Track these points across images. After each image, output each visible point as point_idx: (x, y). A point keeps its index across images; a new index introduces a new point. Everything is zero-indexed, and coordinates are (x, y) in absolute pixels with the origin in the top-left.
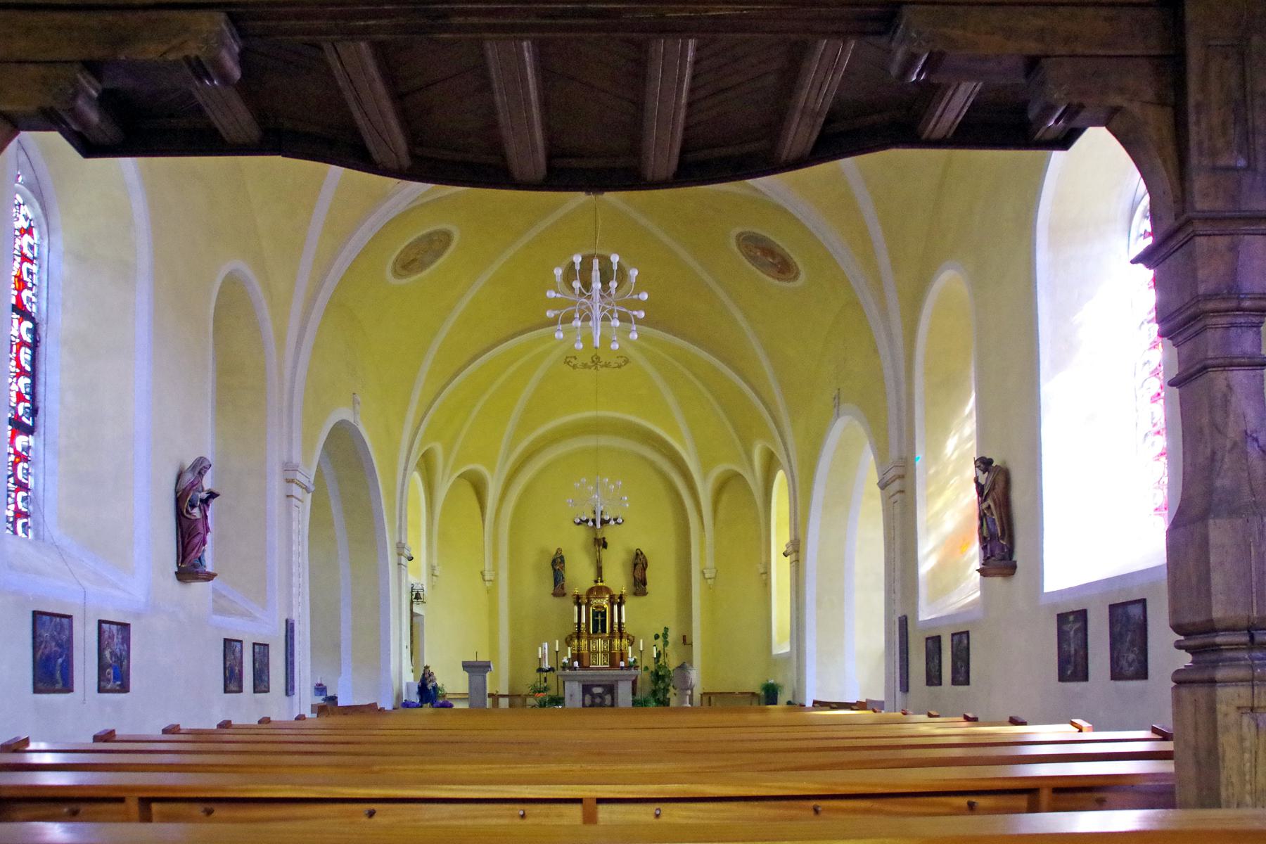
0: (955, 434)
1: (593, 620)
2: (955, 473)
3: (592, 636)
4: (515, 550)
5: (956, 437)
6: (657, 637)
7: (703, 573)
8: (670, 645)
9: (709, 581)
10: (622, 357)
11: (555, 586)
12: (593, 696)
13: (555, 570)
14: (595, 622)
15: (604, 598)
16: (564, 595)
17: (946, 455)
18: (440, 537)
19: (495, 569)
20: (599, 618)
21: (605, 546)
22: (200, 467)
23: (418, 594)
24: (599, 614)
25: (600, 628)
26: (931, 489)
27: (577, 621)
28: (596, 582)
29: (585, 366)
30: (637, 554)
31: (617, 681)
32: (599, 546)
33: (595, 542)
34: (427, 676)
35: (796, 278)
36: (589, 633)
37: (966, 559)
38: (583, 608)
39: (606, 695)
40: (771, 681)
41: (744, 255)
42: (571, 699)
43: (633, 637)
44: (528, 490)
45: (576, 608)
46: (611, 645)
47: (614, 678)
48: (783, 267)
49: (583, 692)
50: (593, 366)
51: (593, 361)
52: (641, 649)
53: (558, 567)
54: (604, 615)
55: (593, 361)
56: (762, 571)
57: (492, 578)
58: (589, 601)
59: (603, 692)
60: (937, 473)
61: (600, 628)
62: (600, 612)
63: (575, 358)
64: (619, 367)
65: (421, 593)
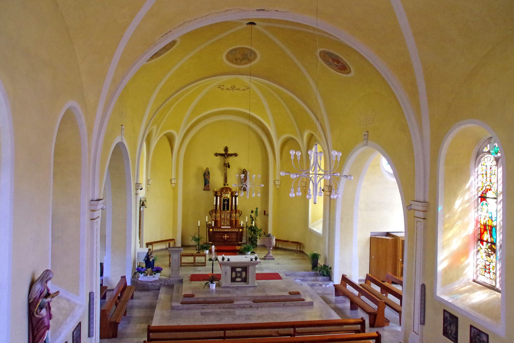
0: (460, 198)
1: (223, 203)
2: (459, 218)
4: (186, 167)
5: (461, 199)
6: (252, 212)
7: (274, 181)
9: (277, 186)
10: (246, 87)
11: (205, 185)
13: (205, 178)
14: (224, 205)
15: (228, 194)
16: (209, 190)
17: (455, 208)
18: (152, 167)
19: (177, 179)
21: (229, 167)
22: (46, 276)
23: (143, 203)
24: (226, 201)
25: (226, 208)
26: (446, 226)
28: (225, 185)
29: (228, 89)
30: (244, 171)
31: (249, 266)
32: (226, 167)
33: (224, 165)
34: (149, 254)
35: (350, 72)
36: (221, 210)
37: (463, 265)
38: (219, 198)
40: (316, 252)
41: (322, 59)
44: (193, 138)
45: (215, 198)
46: (231, 217)
47: (248, 265)
48: (343, 68)
49: (231, 271)
50: (231, 89)
51: (232, 87)
54: (228, 201)
55: (232, 87)
56: (304, 185)
57: (175, 183)
58: (221, 195)
60: (449, 218)
61: (226, 208)
62: (226, 199)
63: (223, 86)
64: (244, 90)
65: (145, 203)
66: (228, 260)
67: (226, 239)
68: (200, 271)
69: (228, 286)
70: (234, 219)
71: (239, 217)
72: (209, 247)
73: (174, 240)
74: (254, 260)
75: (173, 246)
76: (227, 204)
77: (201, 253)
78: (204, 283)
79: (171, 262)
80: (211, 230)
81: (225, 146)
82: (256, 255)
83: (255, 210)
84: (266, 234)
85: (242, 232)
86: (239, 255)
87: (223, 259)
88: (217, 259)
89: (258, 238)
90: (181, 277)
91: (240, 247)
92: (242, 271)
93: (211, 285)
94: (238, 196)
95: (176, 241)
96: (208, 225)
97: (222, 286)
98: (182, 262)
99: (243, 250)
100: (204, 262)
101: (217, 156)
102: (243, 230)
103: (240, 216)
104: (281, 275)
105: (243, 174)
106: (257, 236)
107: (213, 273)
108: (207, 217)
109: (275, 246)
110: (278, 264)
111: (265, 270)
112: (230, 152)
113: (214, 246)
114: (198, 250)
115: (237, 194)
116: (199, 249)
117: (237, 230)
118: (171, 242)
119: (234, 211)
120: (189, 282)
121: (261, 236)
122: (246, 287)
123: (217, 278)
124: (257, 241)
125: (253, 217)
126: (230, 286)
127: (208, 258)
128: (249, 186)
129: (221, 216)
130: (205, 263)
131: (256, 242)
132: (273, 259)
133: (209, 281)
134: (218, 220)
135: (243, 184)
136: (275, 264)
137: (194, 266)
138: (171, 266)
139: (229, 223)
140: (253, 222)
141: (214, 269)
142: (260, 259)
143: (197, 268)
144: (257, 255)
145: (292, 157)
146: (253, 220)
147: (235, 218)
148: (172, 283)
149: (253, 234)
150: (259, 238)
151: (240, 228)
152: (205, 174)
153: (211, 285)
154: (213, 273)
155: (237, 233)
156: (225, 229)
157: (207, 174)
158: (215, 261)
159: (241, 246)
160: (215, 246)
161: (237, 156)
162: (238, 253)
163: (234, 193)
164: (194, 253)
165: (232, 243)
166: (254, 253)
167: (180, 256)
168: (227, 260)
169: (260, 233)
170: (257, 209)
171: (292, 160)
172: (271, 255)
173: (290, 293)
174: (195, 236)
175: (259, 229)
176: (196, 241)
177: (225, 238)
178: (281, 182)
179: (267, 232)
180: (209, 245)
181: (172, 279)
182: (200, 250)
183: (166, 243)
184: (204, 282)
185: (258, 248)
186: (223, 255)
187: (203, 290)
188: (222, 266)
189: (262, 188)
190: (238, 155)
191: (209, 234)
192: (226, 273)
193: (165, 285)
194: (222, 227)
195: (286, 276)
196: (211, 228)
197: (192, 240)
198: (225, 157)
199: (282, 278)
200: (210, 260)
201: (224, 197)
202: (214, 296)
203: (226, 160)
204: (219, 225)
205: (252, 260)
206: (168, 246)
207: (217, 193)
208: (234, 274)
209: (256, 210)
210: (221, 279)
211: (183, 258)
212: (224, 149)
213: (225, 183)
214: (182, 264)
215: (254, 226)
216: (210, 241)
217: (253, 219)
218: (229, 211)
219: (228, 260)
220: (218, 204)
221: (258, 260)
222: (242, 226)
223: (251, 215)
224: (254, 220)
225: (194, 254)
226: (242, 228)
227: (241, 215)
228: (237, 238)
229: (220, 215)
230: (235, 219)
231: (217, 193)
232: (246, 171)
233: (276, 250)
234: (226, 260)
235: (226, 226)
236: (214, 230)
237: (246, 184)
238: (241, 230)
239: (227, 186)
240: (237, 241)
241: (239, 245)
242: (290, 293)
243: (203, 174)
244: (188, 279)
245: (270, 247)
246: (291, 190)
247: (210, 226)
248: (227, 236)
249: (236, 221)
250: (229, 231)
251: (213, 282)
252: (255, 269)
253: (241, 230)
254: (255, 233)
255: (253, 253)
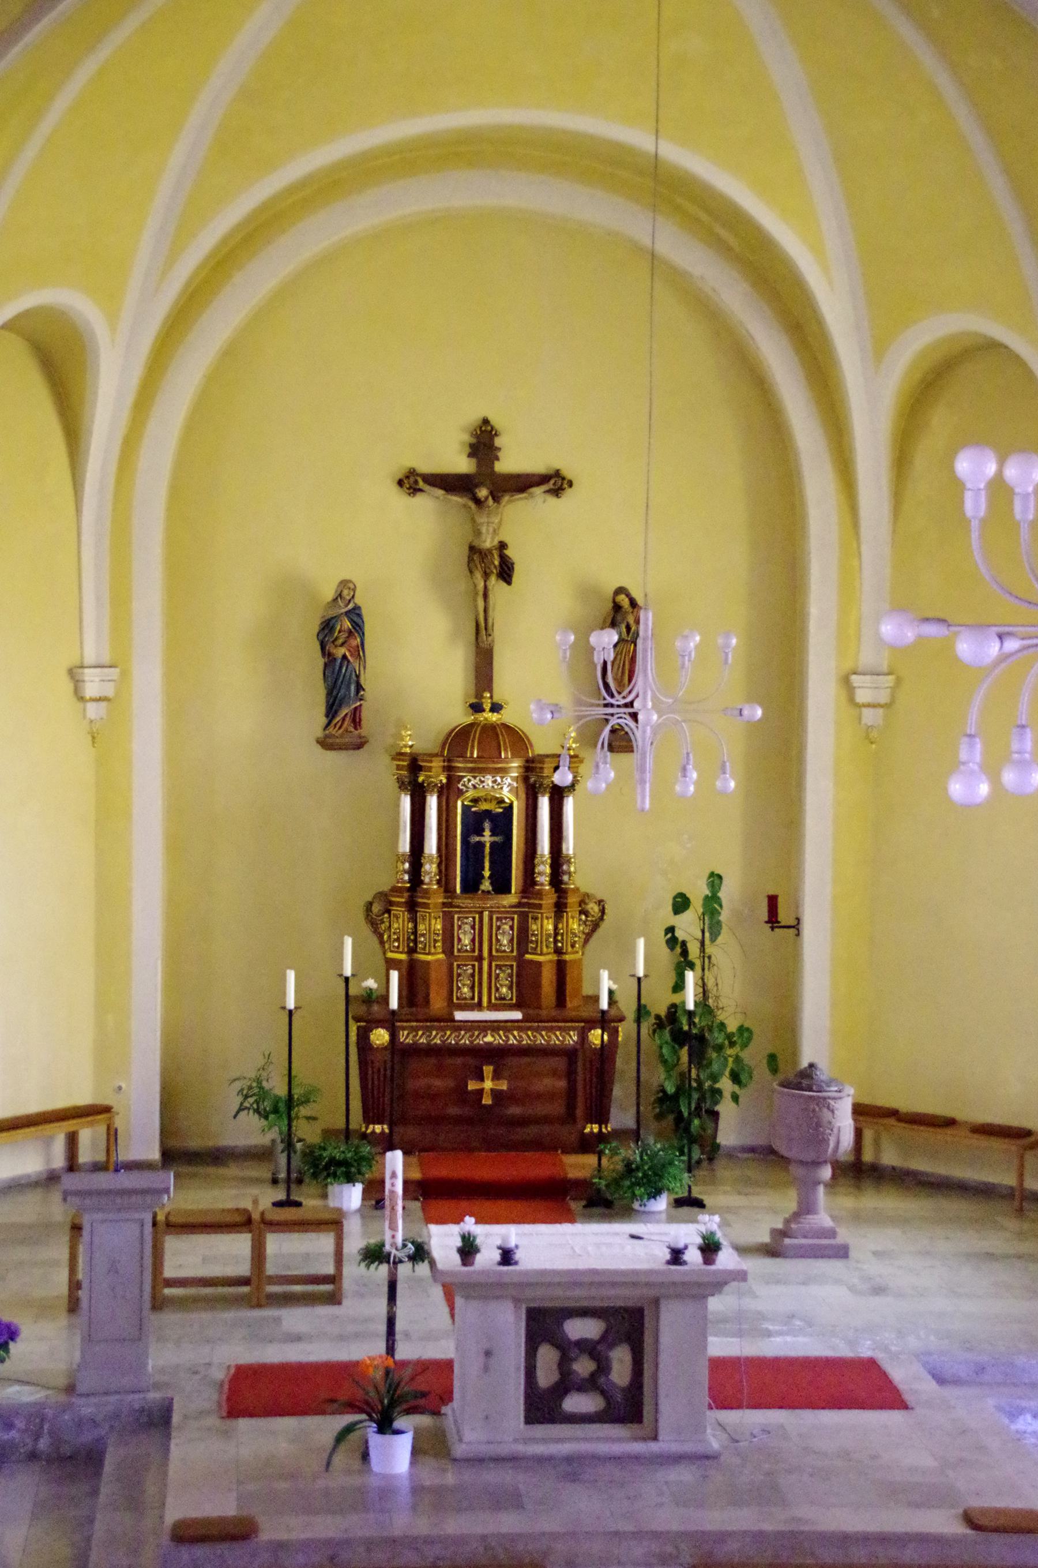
3: (457, 902)
6: (681, 904)
7: (846, 681)
8: (725, 930)
9: (866, 711)
11: (332, 710)
12: (567, 1350)
13: (330, 660)
14: (473, 853)
15: (503, 771)
20: (487, 838)
21: (506, 572)
24: (487, 825)
25: (487, 873)
27: (407, 848)
30: (617, 607)
31: (656, 1302)
32: (486, 575)
33: (470, 560)
38: (432, 802)
39: (612, 1346)
42: (486, 1369)
43: (600, 902)
45: (406, 802)
46: (523, 938)
47: (652, 1293)
52: (641, 973)
53: (340, 652)
54: (502, 821)
58: (452, 780)
59: (604, 1337)
61: (487, 873)
62: (488, 813)
66: (507, 1256)
67: (487, 1101)
68: (298, 1338)
69: (504, 1450)
70: (546, 958)
71: (586, 941)
72: (368, 1160)
73: (107, 1110)
74: (694, 1256)
75: (101, 1157)
76: (493, 845)
77: (311, 1203)
78: (327, 1426)
79: (80, 1276)
80: (380, 1036)
81: (472, 416)
82: (709, 1222)
83: (698, 891)
84: (781, 1066)
85: (606, 1054)
86: (589, 1218)
87: (468, 1250)
88: (420, 1253)
89: (727, 1094)
90: (157, 1386)
91: (591, 1160)
92: (607, 1340)
93: (376, 1441)
94: (572, 787)
95: (118, 1122)
96: (356, 997)
97: (459, 1450)
98: (169, 1272)
99: (616, 1182)
100: (330, 1269)
101: (414, 490)
102: (614, 1033)
103: (588, 937)
104: (898, 1374)
105: (613, 624)
106: (715, 1078)
107: (391, 1350)
108: (348, 942)
109: (851, 1158)
110: (879, 1290)
111: (780, 1333)
112: (508, 463)
113: (398, 1154)
114: (288, 1180)
115: (562, 777)
116: (294, 1175)
117: (572, 1038)
118: (91, 1124)
119: (549, 900)
120: (213, 1421)
121: (743, 1077)
122: (637, 1458)
123: (424, 1395)
124: (715, 1115)
125: (684, 944)
126: (521, 1448)
127: (355, 1241)
128: (655, 717)
129: (449, 937)
130: (334, 1279)
131: (710, 1125)
132: (842, 1252)
133: (364, 1416)
134: (433, 967)
135: (609, 700)
136: (852, 1289)
137: (254, 1301)
138: (84, 1304)
139: (510, 988)
140: (690, 976)
141: (399, 1326)
142: (742, 1250)
143: (278, 1320)
144: (717, 1218)
145: (975, 506)
146: (684, 963)
147: (558, 951)
148: (87, 1437)
149: (690, 1062)
150: (735, 1098)
151: (591, 1024)
152: (327, 627)
153: (376, 1441)
154: (391, 1350)
155: (570, 1054)
156: (486, 1026)
157: (347, 624)
158: (409, 1265)
159: (600, 1154)
160: (406, 1153)
161: (569, 492)
162: (576, 1206)
163: (548, 766)
164: (255, 1202)
165: (531, 1131)
166: (699, 1204)
167: (148, 1228)
168: (497, 1256)
169: (738, 1059)
170: (715, 880)
171: (975, 524)
172: (823, 1219)
173: (969, 1519)
174: (259, 1081)
175: (732, 1027)
176: (272, 1117)
177: (480, 1092)
178: (899, 681)
179: (795, 1052)
180: (366, 1149)
181: (87, 1408)
182: (300, 1181)
183: (48, 1141)
184: (329, 1418)
185: (723, 1170)
186: (469, 1220)
187: (321, 1483)
188: (459, 1301)
189: (754, 726)
190: (570, 484)
191: (363, 1064)
192: (488, 1354)
193: (33, 1456)
194: (459, 1015)
195: (933, 1384)
196: (379, 1023)
197: (241, 1109)
198: (478, 502)
199: (908, 1397)
200: (374, 1255)
201: (470, 794)
202: (397, 1532)
203: (482, 519)
204: (438, 1003)
205: (676, 1256)
206: (59, 1161)
207: (420, 769)
208: (547, 1356)
209: (708, 892)
210: (456, 1395)
211: (172, 1244)
212: (467, 438)
213: (479, 695)
214: (168, 1291)
215: (691, 1006)
216: (370, 1117)
217: (685, 952)
218: (511, 899)
219: (507, 1256)
220: (427, 851)
221: (726, 1259)
222: (604, 1005)
223: (671, 930)
224: (691, 966)
225: (256, 1216)
226: (605, 1021)
227: (596, 926)
228: (571, 1093)
229: (444, 929)
230: (555, 957)
231: (420, 769)
232: (633, 604)
233: (858, 1188)
234: (487, 1257)
235: (492, 1007)
236: (405, 1037)
237: (631, 704)
238: (596, 1036)
239: (494, 717)
240: (570, 1116)
241: (587, 1145)
242: (969, 1519)
243: (316, 629)
244: (209, 1398)
245: (817, 1164)
246: (963, 756)
247: (375, 1008)
248: (497, 1076)
249: (561, 968)
250: (512, 1041)
251: (391, 1421)
252: (701, 1327)
253: (596, 1036)
254: (698, 1057)
255: (690, 1203)
